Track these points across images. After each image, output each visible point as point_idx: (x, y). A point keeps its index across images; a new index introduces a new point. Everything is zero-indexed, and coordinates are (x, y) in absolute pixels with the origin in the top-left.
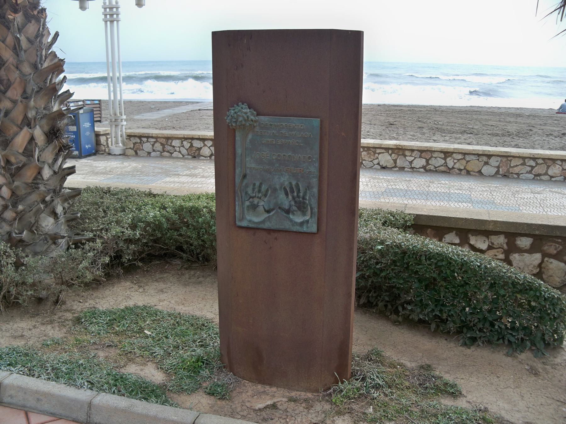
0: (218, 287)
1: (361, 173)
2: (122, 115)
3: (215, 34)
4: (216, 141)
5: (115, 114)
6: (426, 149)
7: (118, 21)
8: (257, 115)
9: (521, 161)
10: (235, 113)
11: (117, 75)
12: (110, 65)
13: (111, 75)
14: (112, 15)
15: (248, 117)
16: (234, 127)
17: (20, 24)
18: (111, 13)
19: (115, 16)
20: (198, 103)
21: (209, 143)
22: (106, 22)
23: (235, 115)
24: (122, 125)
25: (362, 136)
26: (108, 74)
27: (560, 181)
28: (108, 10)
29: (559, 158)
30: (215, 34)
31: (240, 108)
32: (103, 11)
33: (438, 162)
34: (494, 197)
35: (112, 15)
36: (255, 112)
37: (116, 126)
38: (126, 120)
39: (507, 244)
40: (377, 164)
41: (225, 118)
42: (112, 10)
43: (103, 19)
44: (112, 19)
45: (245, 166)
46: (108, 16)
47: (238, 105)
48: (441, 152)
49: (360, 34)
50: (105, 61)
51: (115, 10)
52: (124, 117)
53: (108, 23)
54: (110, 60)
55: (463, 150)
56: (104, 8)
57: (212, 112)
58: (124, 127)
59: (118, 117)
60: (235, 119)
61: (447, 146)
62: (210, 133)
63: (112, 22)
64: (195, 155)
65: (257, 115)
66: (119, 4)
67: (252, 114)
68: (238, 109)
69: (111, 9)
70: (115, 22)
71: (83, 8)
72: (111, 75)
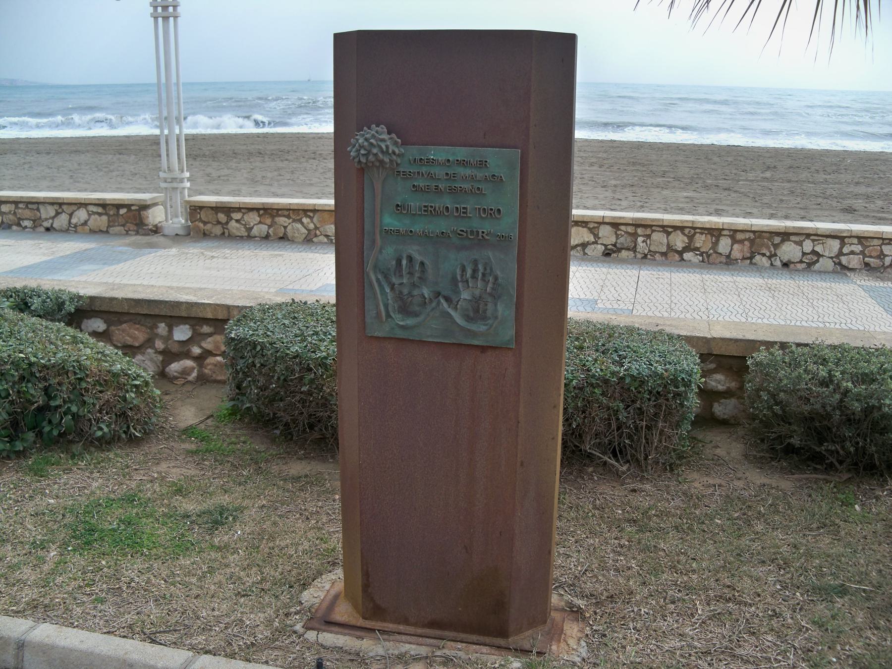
1: (571, 263)
2: (182, 171)
3: (340, 39)
7: (176, 17)
8: (402, 144)
10: (366, 140)
11: (177, 131)
12: (163, 88)
13: (166, 132)
15: (387, 147)
16: (363, 165)
19: (171, 9)
20: (366, 575)
22: (156, 18)
25: (574, 205)
26: (162, 132)
30: (340, 39)
36: (399, 141)
37: (166, 19)
38: (189, 180)
43: (151, 3)
44: (165, 14)
45: (381, 222)
46: (160, 9)
47: (369, 128)
50: (155, 81)
52: (187, 175)
53: (160, 20)
54: (163, 80)
60: (365, 150)
62: (329, 202)
63: (166, 19)
65: (402, 144)
67: (396, 143)
68: (369, 133)
70: (171, 19)
72: (166, 132)
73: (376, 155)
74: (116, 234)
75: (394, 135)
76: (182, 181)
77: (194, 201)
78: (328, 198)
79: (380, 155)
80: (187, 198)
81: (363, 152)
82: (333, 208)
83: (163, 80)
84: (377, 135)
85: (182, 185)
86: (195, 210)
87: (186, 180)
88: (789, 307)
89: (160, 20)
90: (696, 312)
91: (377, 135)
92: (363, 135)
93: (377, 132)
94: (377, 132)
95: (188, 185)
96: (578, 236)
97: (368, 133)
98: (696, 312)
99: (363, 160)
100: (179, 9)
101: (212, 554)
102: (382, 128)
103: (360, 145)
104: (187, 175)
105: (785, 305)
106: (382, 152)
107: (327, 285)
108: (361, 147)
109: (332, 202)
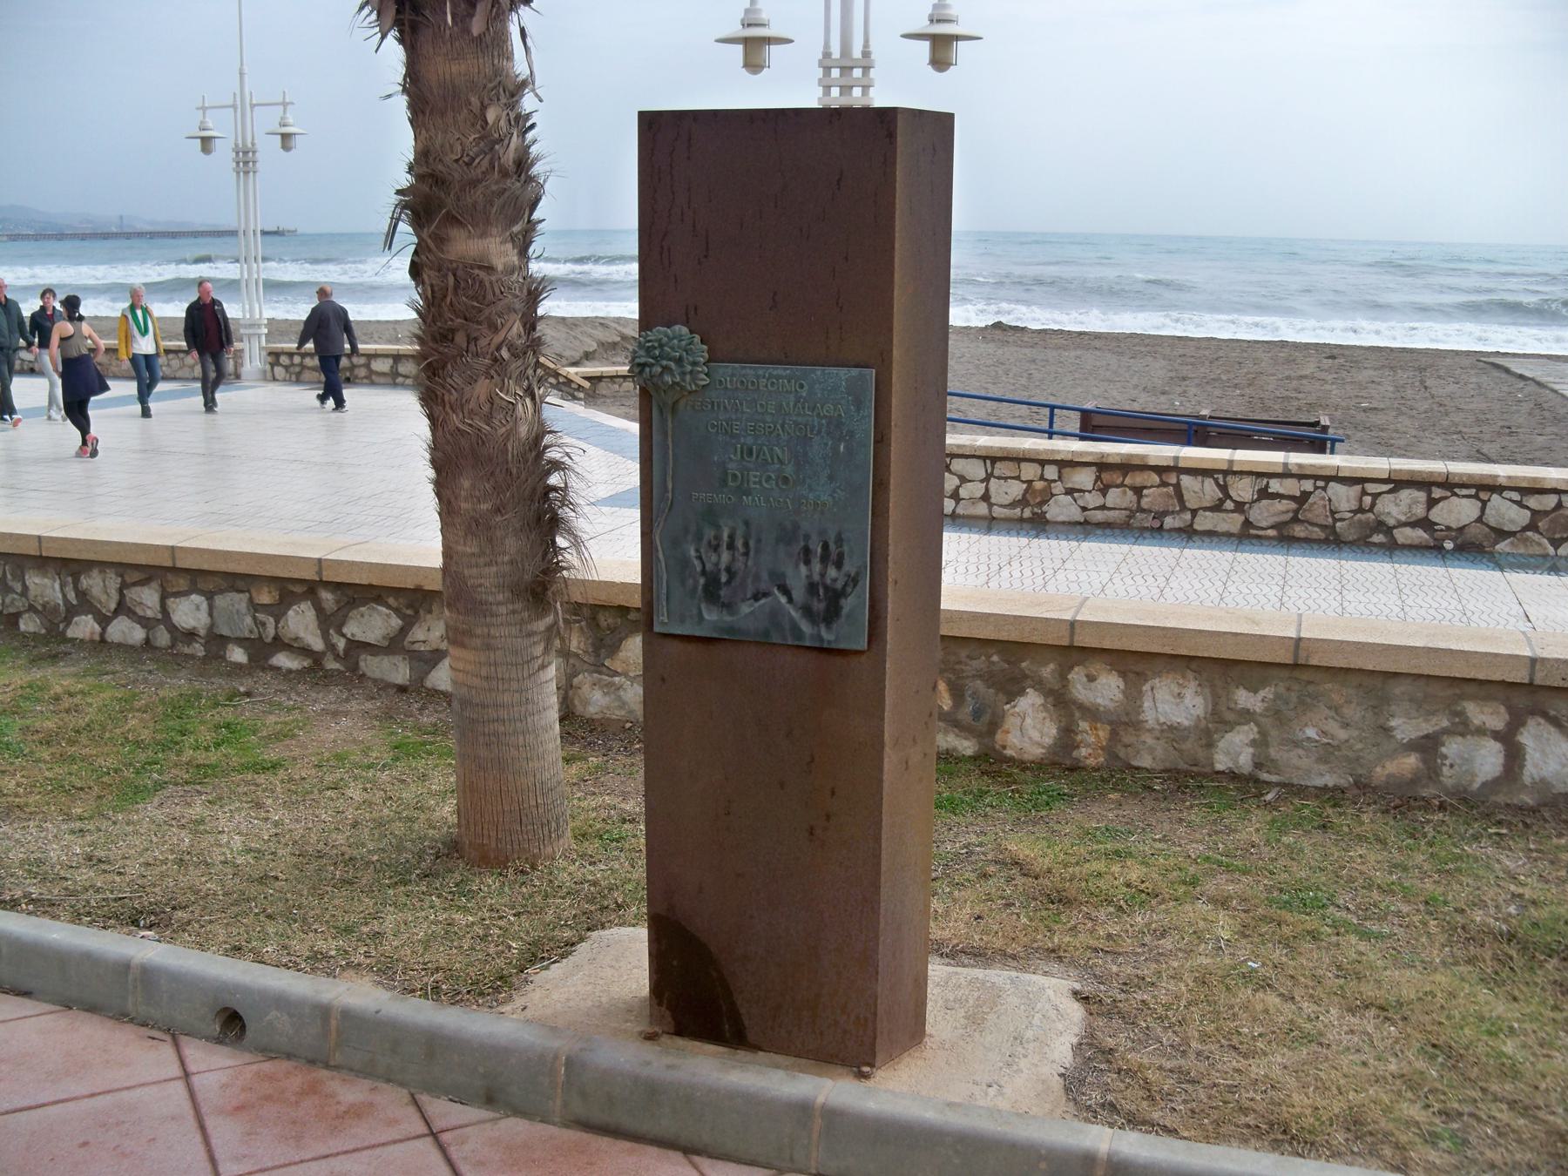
0: (647, 752)
7: (254, 172)
9: (1155, 479)
11: (256, 276)
13: (246, 276)
14: (246, 163)
22: (238, 173)
28: (835, 73)
33: (1458, 511)
34: (1344, 572)
35: (246, 163)
39: (557, 551)
40: (1104, 496)
42: (850, 94)
44: (246, 169)
53: (242, 174)
55: (1322, 467)
56: (824, 68)
61: (1034, 443)
63: (247, 173)
69: (846, 70)
70: (251, 174)
83: (239, 103)
85: (259, 331)
89: (242, 174)
100: (257, 154)
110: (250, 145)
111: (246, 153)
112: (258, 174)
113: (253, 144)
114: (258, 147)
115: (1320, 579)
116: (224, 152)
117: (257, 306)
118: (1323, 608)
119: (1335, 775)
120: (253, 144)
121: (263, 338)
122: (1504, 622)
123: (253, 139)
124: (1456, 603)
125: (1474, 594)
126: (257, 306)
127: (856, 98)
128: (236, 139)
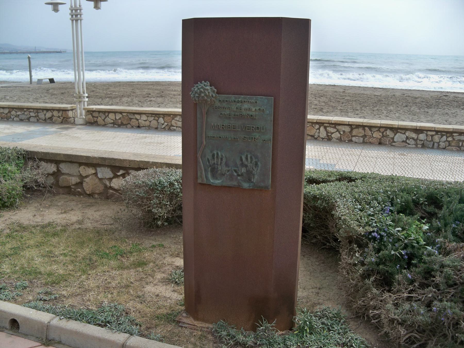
1: (307, 144)
4: (184, 115)
5: (79, 93)
6: (51, 108)
7: (81, 20)
10: (199, 89)
17: (60, 211)
18: (76, 14)
21: (178, 118)
22: (72, 21)
23: (198, 91)
24: (85, 101)
27: (412, 148)
29: (26, 107)
31: (203, 85)
32: (70, 12)
35: (76, 16)
36: (216, 90)
38: (87, 97)
41: (190, 93)
44: (76, 18)
47: (201, 83)
48: (349, 125)
49: (309, 21)
51: (79, 11)
53: (74, 21)
54: (76, 51)
57: (180, 88)
58: (86, 103)
59: (81, 95)
63: (77, 21)
64: (169, 129)
66: (82, 7)
67: (214, 91)
68: (200, 85)
70: (79, 21)
71: (97, 7)
73: (203, 97)
74: (10, 121)
75: (213, 88)
76: (84, 97)
77: (90, 108)
78: (176, 107)
79: (206, 98)
80: (86, 107)
81: (197, 95)
82: (181, 114)
83: (76, 51)
84: (204, 87)
86: (90, 112)
87: (86, 97)
88: (455, 168)
90: (419, 172)
91: (204, 87)
92: (197, 87)
93: (204, 85)
94: (204, 85)
95: (87, 99)
96: (309, 130)
97: (200, 85)
98: (419, 172)
99: (197, 99)
100: (82, 16)
101: (114, 272)
102: (207, 83)
103: (195, 92)
104: (86, 95)
105: (453, 167)
106: (207, 96)
107: (177, 155)
108: (196, 93)
109: (180, 110)
110: (78, 6)
111: (76, 10)
112: (82, 21)
113: (80, 6)
114: (83, 7)
115: (405, 167)
116: (65, 11)
117: (82, 73)
118: (403, 171)
119: (16, 168)
120: (80, 6)
121: (86, 103)
122: (445, 177)
123: (80, 4)
124: (431, 174)
125: (457, 172)
126: (82, 73)
127: (311, 64)
128: (71, 4)
